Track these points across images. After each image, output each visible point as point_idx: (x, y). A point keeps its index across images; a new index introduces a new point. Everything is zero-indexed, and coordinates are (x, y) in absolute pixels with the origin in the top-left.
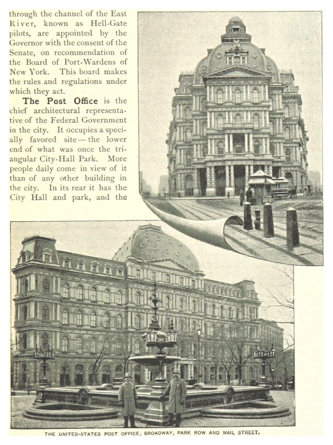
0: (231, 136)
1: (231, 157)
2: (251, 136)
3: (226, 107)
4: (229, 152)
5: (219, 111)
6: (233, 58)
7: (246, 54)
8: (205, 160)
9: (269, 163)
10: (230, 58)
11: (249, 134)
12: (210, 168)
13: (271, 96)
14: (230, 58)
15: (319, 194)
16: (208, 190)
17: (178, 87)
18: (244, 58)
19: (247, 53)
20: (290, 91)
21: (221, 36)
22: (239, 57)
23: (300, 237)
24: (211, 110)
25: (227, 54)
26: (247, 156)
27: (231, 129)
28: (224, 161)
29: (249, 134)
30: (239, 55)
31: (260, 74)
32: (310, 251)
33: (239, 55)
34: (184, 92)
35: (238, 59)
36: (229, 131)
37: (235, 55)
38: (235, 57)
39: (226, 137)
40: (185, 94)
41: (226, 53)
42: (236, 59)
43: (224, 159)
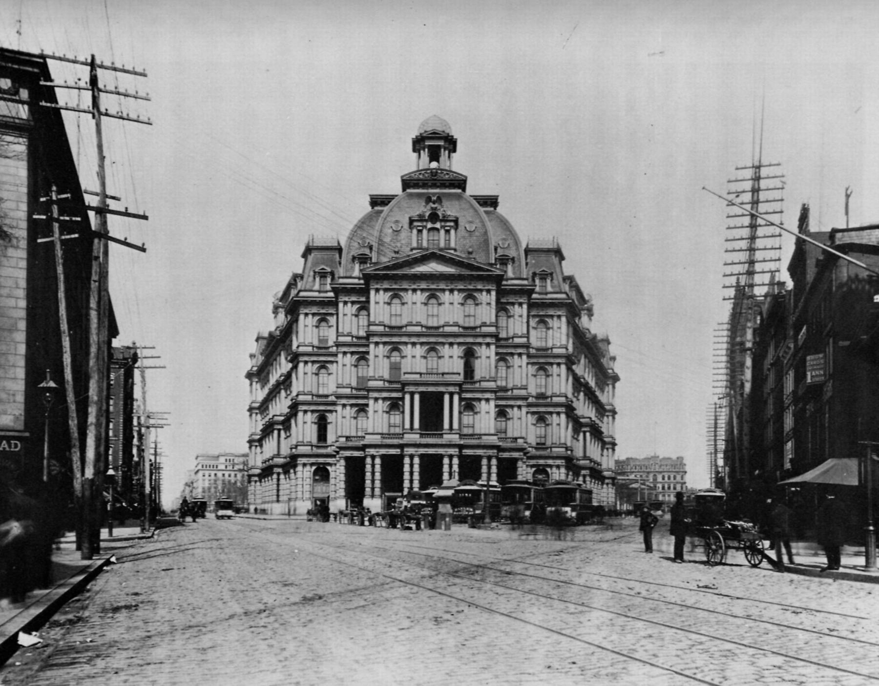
0: (417, 397)
1: (415, 438)
2: (456, 398)
3: (410, 335)
4: (412, 428)
5: (393, 343)
6: (425, 232)
7: (452, 224)
8: (362, 443)
9: (491, 452)
10: (420, 231)
11: (451, 394)
12: (373, 457)
13: (502, 308)
14: (420, 231)
15: (473, 526)
16: (367, 502)
17: (300, 272)
18: (448, 232)
19: (456, 221)
20: (549, 289)
21: (402, 177)
22: (437, 230)
23: (85, 195)
24: (376, 339)
25: (416, 224)
26: (448, 438)
27: (416, 384)
28: (402, 447)
29: (451, 394)
30: (438, 225)
31: (479, 269)
32: (563, 632)
33: (438, 225)
34: (317, 287)
35: (436, 233)
36: (412, 389)
37: (430, 225)
38: (430, 230)
39: (407, 397)
40: (319, 292)
41: (411, 221)
42: (431, 233)
43: (401, 442)
